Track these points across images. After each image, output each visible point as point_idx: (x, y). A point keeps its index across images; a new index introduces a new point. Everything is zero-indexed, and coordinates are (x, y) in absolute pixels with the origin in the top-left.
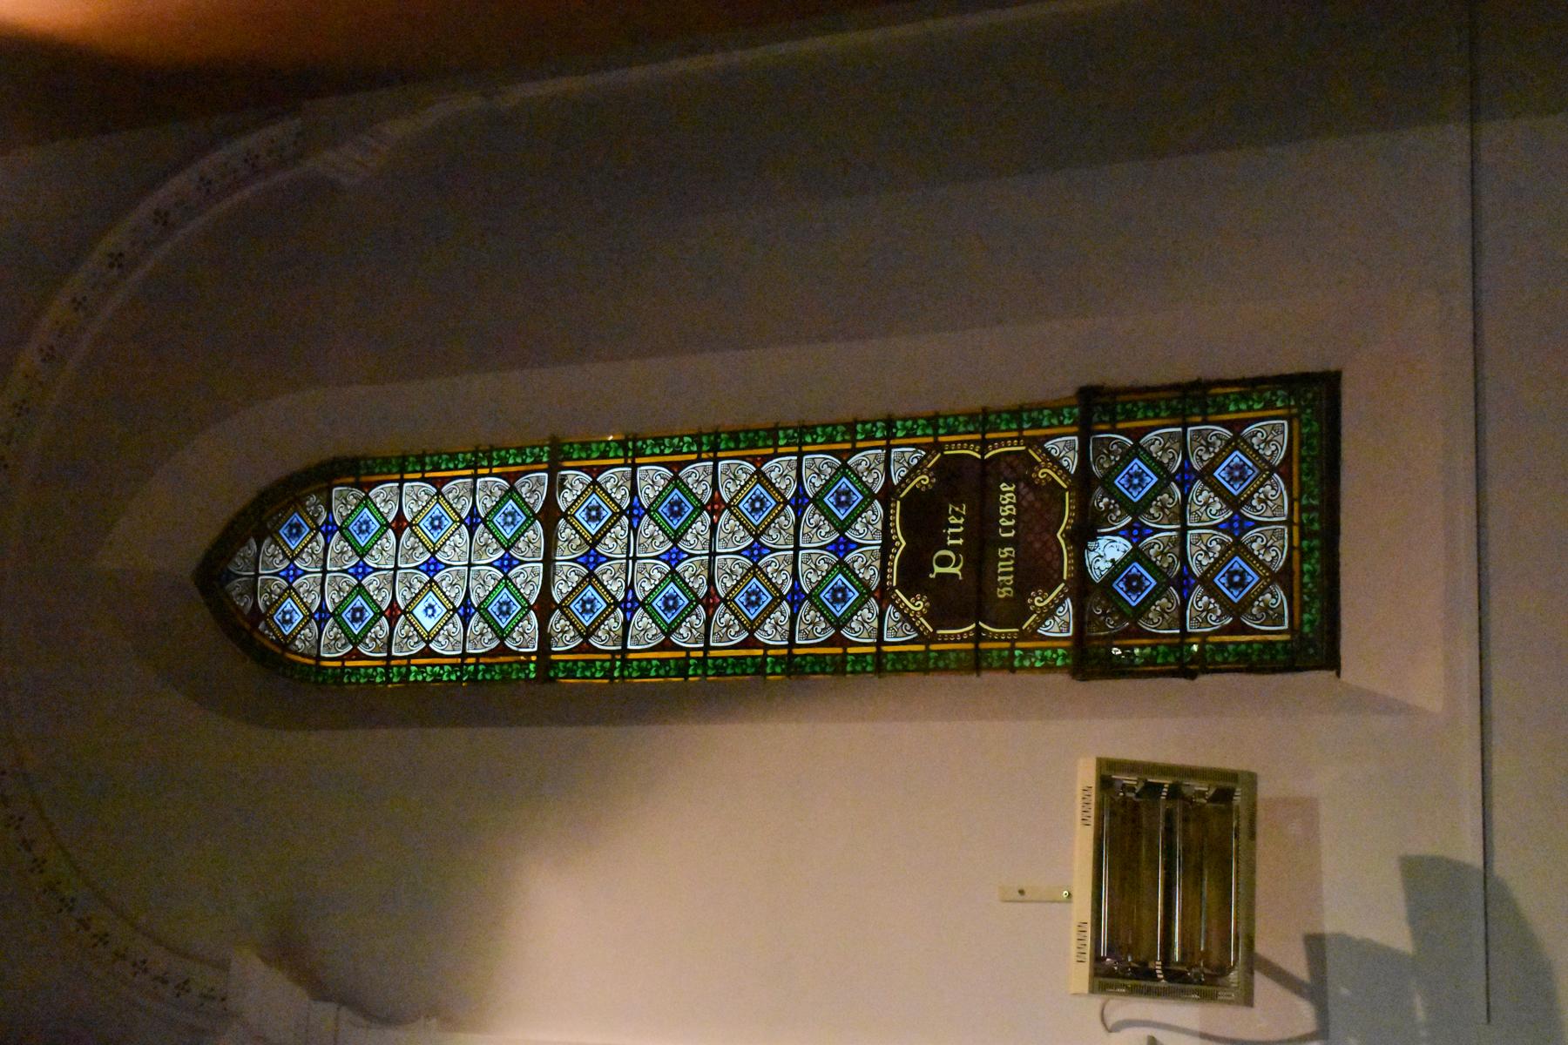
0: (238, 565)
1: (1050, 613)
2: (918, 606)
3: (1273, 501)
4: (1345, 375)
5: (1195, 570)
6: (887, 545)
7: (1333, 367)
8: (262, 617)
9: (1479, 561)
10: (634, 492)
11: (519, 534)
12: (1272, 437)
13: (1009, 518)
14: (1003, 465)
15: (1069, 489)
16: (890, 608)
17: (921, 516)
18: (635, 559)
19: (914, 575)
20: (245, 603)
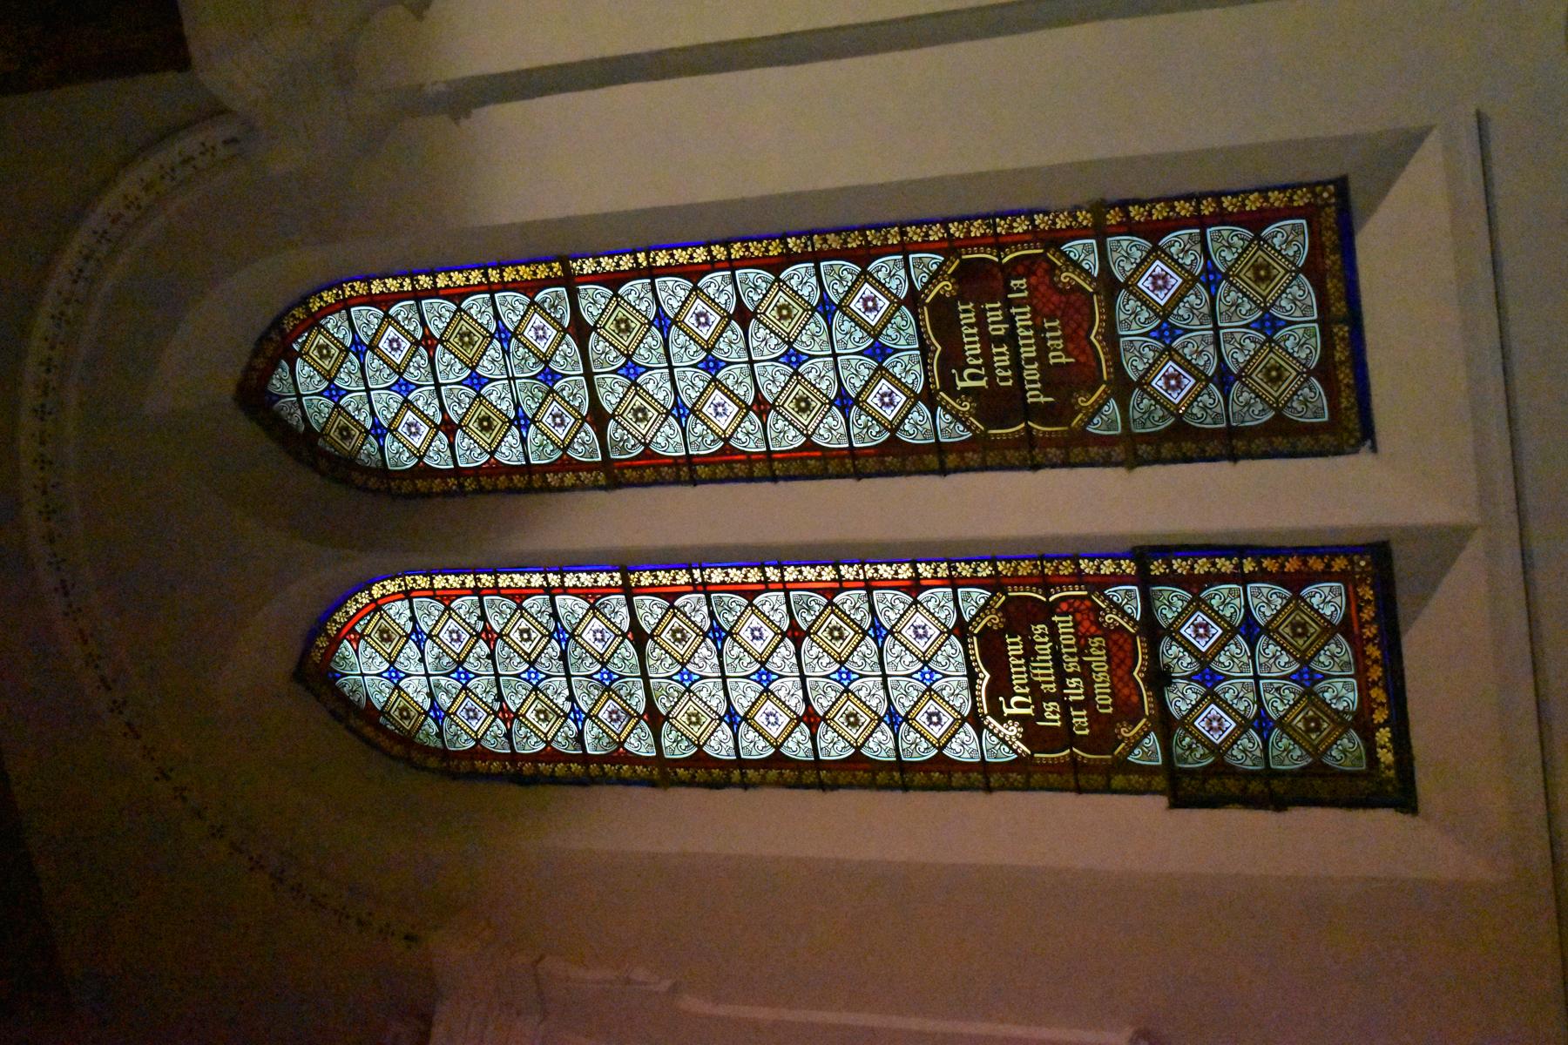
3: (1297, 301)
15: (1096, 292)
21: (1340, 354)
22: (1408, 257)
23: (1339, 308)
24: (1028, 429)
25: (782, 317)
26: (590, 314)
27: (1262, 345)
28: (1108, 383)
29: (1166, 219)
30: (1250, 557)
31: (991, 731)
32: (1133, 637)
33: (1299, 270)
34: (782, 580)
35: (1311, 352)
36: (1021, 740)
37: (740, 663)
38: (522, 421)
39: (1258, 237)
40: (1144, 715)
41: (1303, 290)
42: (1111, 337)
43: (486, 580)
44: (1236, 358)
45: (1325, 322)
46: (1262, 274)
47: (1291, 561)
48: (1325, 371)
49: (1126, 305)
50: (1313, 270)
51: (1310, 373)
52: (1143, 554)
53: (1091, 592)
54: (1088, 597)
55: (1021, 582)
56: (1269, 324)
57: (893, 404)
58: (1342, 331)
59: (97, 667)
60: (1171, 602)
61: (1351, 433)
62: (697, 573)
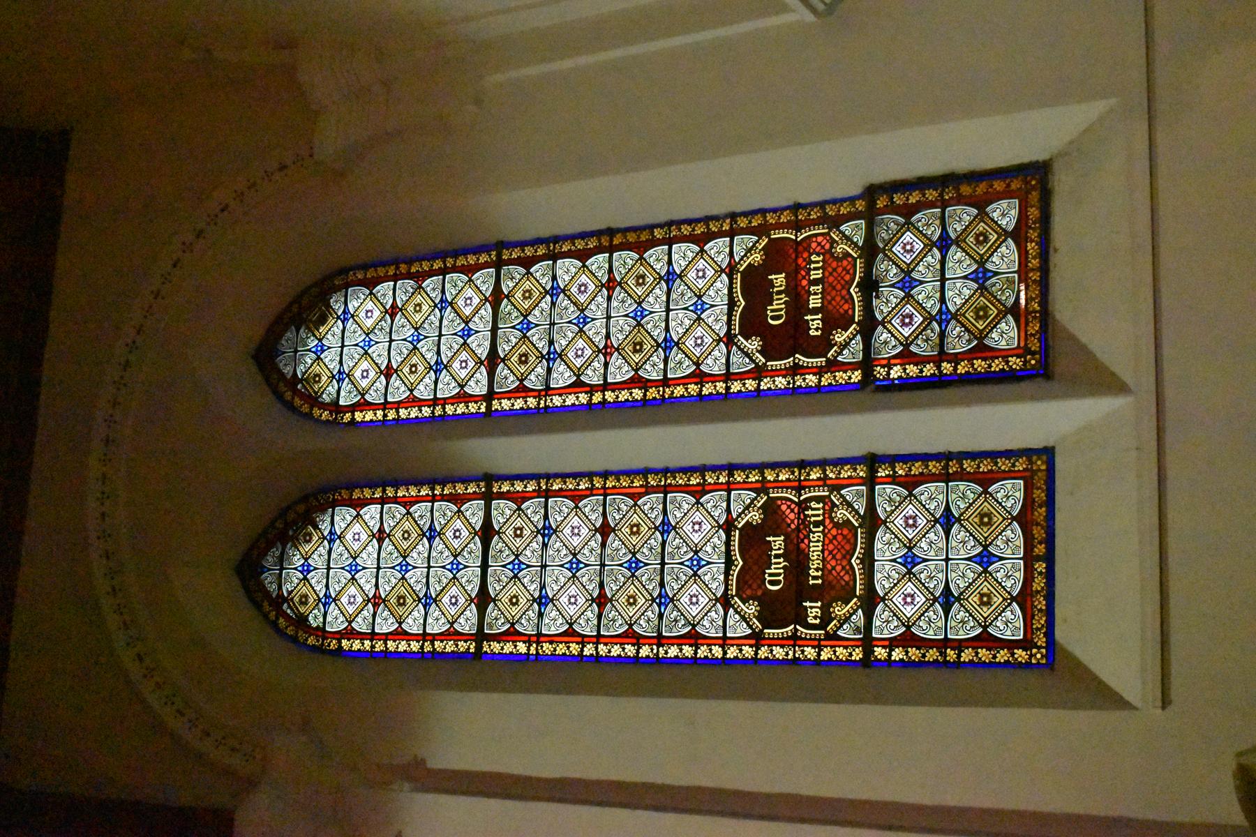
0: (285, 344)
1: (846, 345)
2: (751, 609)
3: (1010, 543)
4: (1057, 450)
5: (951, 308)
6: (732, 304)
7: (1050, 444)
8: (285, 600)
9: (1153, 232)
10: (554, 278)
11: (476, 311)
12: (1010, 493)
13: (817, 570)
14: (814, 245)
15: (860, 257)
16: (731, 611)
17: (754, 285)
18: (554, 324)
19: (753, 323)
20: (288, 370)
21: (1039, 583)
22: (1088, 226)
23: (1040, 549)
24: (796, 630)
25: (632, 533)
26: (497, 520)
27: (980, 575)
28: (859, 598)
29: (921, 474)
30: (948, 465)
31: (739, 347)
32: (855, 259)
33: (1013, 519)
34: (604, 488)
35: (1014, 584)
36: (756, 617)
37: (558, 552)
38: (428, 601)
39: (985, 492)
40: (853, 322)
41: (1015, 534)
42: (869, 561)
43: (390, 492)
44: (958, 584)
45: (1029, 559)
46: (985, 519)
47: (980, 467)
48: (1024, 599)
49: (882, 537)
50: (1024, 519)
51: (1013, 599)
52: (872, 461)
53: (830, 229)
54: (828, 233)
55: (780, 226)
56: (985, 559)
57: (702, 604)
58: (1041, 567)
59: (103, 493)
60: (886, 492)
61: (1039, 648)
62: (533, 651)
